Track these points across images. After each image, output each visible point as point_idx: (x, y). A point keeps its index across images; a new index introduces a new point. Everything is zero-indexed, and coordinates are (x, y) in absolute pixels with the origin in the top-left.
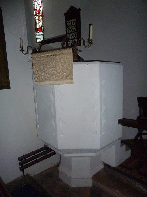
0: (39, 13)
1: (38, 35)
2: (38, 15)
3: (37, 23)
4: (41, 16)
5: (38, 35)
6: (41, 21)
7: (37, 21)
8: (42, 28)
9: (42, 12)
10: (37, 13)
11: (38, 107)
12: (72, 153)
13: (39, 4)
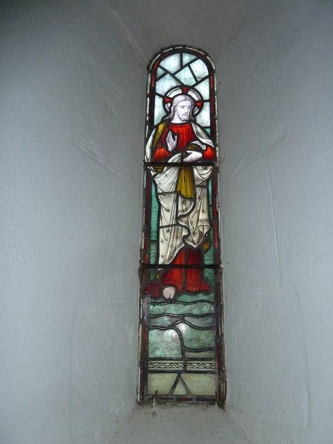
0: (182, 148)
1: (166, 321)
2: (175, 158)
3: (167, 218)
4: (204, 162)
5: (166, 321)
6: (202, 204)
7: (167, 203)
8: (208, 259)
9: (212, 136)
10: (171, 143)
11: (147, 140)
12: (164, 360)
13: (185, 89)
